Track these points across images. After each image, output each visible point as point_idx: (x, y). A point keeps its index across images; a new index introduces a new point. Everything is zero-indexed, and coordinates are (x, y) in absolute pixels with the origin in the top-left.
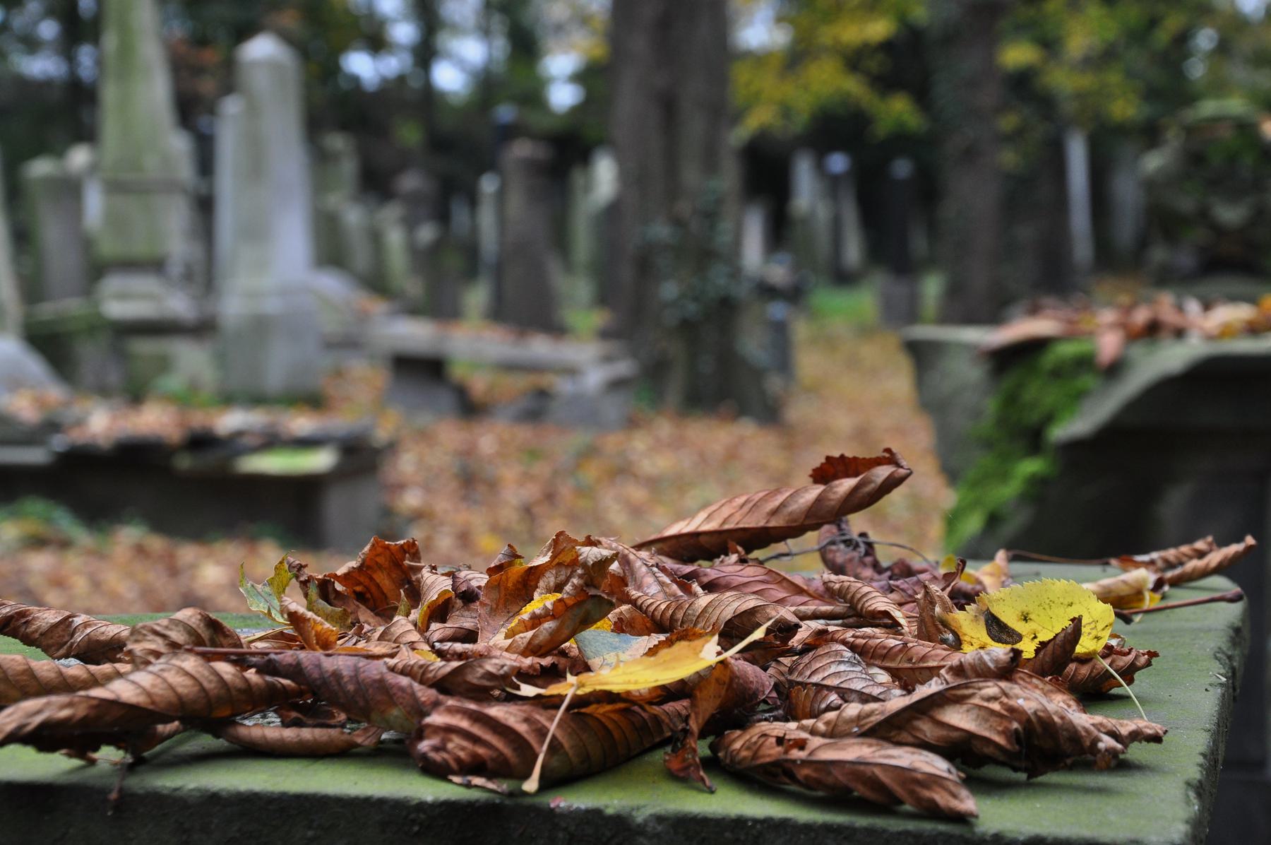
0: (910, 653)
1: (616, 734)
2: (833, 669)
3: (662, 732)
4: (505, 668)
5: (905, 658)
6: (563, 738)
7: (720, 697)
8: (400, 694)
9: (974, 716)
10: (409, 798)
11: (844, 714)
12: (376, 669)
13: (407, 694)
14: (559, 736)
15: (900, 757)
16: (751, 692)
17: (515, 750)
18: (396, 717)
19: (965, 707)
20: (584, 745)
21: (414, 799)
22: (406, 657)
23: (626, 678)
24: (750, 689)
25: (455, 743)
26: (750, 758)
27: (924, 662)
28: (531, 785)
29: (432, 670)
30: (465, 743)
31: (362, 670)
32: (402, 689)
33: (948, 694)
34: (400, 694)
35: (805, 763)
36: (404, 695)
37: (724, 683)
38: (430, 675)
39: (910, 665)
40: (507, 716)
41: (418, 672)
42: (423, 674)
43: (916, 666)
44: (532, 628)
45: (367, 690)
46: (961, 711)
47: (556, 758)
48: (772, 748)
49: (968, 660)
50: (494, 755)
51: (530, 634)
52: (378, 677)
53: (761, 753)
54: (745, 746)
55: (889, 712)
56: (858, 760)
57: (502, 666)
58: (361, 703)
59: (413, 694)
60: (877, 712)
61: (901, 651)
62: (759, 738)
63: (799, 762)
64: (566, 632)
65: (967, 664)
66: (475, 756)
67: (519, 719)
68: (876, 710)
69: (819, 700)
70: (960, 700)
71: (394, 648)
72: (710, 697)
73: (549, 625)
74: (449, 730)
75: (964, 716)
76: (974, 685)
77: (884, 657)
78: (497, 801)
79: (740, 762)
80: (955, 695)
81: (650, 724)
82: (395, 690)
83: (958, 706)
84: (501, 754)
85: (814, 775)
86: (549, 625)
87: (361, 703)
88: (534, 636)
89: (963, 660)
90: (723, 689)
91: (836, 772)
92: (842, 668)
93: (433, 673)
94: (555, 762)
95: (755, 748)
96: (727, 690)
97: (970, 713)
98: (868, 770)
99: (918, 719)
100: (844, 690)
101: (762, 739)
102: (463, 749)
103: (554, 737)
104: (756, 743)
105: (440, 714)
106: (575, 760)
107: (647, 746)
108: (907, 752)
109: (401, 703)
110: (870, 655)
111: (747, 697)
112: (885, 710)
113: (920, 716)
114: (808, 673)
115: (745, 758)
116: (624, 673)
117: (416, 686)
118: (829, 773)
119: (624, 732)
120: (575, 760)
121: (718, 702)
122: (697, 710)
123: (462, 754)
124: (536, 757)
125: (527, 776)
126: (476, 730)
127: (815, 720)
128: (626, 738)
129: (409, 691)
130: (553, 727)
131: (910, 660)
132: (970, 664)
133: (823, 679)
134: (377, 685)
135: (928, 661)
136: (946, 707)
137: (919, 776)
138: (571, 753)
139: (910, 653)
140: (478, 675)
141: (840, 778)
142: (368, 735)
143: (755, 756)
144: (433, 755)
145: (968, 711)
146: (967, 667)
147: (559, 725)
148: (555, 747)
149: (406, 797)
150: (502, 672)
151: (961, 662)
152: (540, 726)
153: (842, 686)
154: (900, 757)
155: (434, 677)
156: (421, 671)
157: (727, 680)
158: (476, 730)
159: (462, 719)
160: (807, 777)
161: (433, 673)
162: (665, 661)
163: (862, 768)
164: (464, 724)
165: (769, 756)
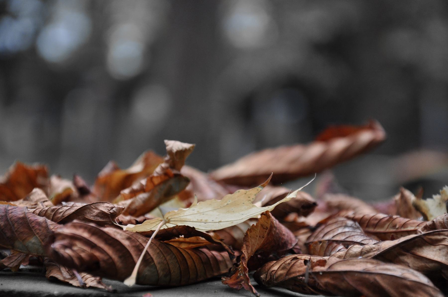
0: (394, 222)
1: (189, 262)
2: (340, 230)
3: (219, 269)
4: (114, 209)
5: (391, 226)
6: (153, 255)
7: (263, 237)
8: (37, 227)
9: (445, 253)
10: (41, 292)
11: (351, 252)
12: (20, 211)
13: (43, 227)
14: (151, 252)
15: (394, 270)
16: (283, 241)
17: (120, 257)
18: (34, 243)
19: (438, 247)
20: (168, 263)
21: (44, 293)
22: (41, 207)
23: (199, 217)
24: (283, 239)
25: (79, 246)
26: (285, 275)
27: (404, 228)
28: (130, 282)
29: (61, 212)
30: (85, 248)
31: (10, 211)
32: (39, 224)
33: (425, 238)
34: (37, 227)
35: (325, 273)
36: (40, 228)
37: (267, 228)
38: (60, 215)
39: (394, 230)
40: (116, 234)
41: (51, 214)
42: (55, 215)
43: (399, 230)
44: (131, 197)
45: (13, 225)
46: (435, 250)
47: (148, 268)
48: (301, 266)
49: (439, 220)
50: (106, 258)
51: (129, 202)
52: (22, 216)
53: (293, 270)
54: (282, 267)
55: (383, 249)
56: (364, 271)
57: (112, 208)
58: (9, 234)
59: (47, 227)
60: (375, 249)
61: (388, 221)
62: (291, 261)
63: (321, 274)
64: (154, 201)
65: (438, 223)
66: (92, 256)
67: (124, 237)
68: (374, 248)
69: (330, 249)
70: (434, 243)
71: (32, 205)
72: (257, 236)
73: (143, 196)
74: (74, 238)
75: (437, 253)
76: (444, 233)
77: (375, 226)
78: (105, 295)
79: (277, 278)
80: (431, 239)
81: (211, 262)
82: (33, 224)
83: (432, 247)
84: (110, 258)
85: (332, 282)
86: (143, 196)
87: (9, 234)
88: (132, 203)
89: (435, 220)
90: (266, 232)
91: (348, 279)
92: (347, 230)
93: (62, 214)
94: (147, 272)
95: (288, 267)
96: (268, 234)
97: (442, 251)
98: (371, 278)
99: (404, 255)
100: (349, 243)
101: (294, 261)
102: (84, 251)
103: (147, 252)
104: (289, 264)
105: (67, 228)
106: (161, 273)
107: (209, 277)
108: (400, 268)
109: (38, 233)
110: (366, 225)
111: (280, 244)
112: (381, 248)
113: (406, 253)
114: (321, 235)
115: (281, 275)
116: (199, 213)
117: (49, 222)
118: (343, 280)
119: (194, 262)
120: (161, 273)
121: (262, 241)
122: (248, 244)
123: (83, 255)
124: (135, 264)
125: (128, 274)
126: (94, 240)
127: (329, 257)
128: (195, 266)
129: (44, 225)
130: (147, 246)
131: (394, 226)
132: (440, 222)
133: (334, 237)
134: (21, 221)
135: (407, 227)
136: (424, 248)
137: (408, 283)
138: (158, 266)
139: (394, 222)
140: (94, 214)
141: (351, 283)
142: (11, 261)
143: (288, 273)
144: (62, 251)
145: (440, 250)
146: (438, 224)
147: (150, 246)
148: (147, 260)
149: (39, 292)
150: (111, 211)
151: (433, 222)
152: (138, 243)
153: (348, 240)
154: (394, 270)
155: (63, 216)
156: (53, 213)
157: (269, 226)
158: (94, 240)
159: (84, 232)
160: (326, 284)
161: (62, 214)
162: (228, 204)
163: (367, 276)
164: (86, 235)
165: (299, 271)
